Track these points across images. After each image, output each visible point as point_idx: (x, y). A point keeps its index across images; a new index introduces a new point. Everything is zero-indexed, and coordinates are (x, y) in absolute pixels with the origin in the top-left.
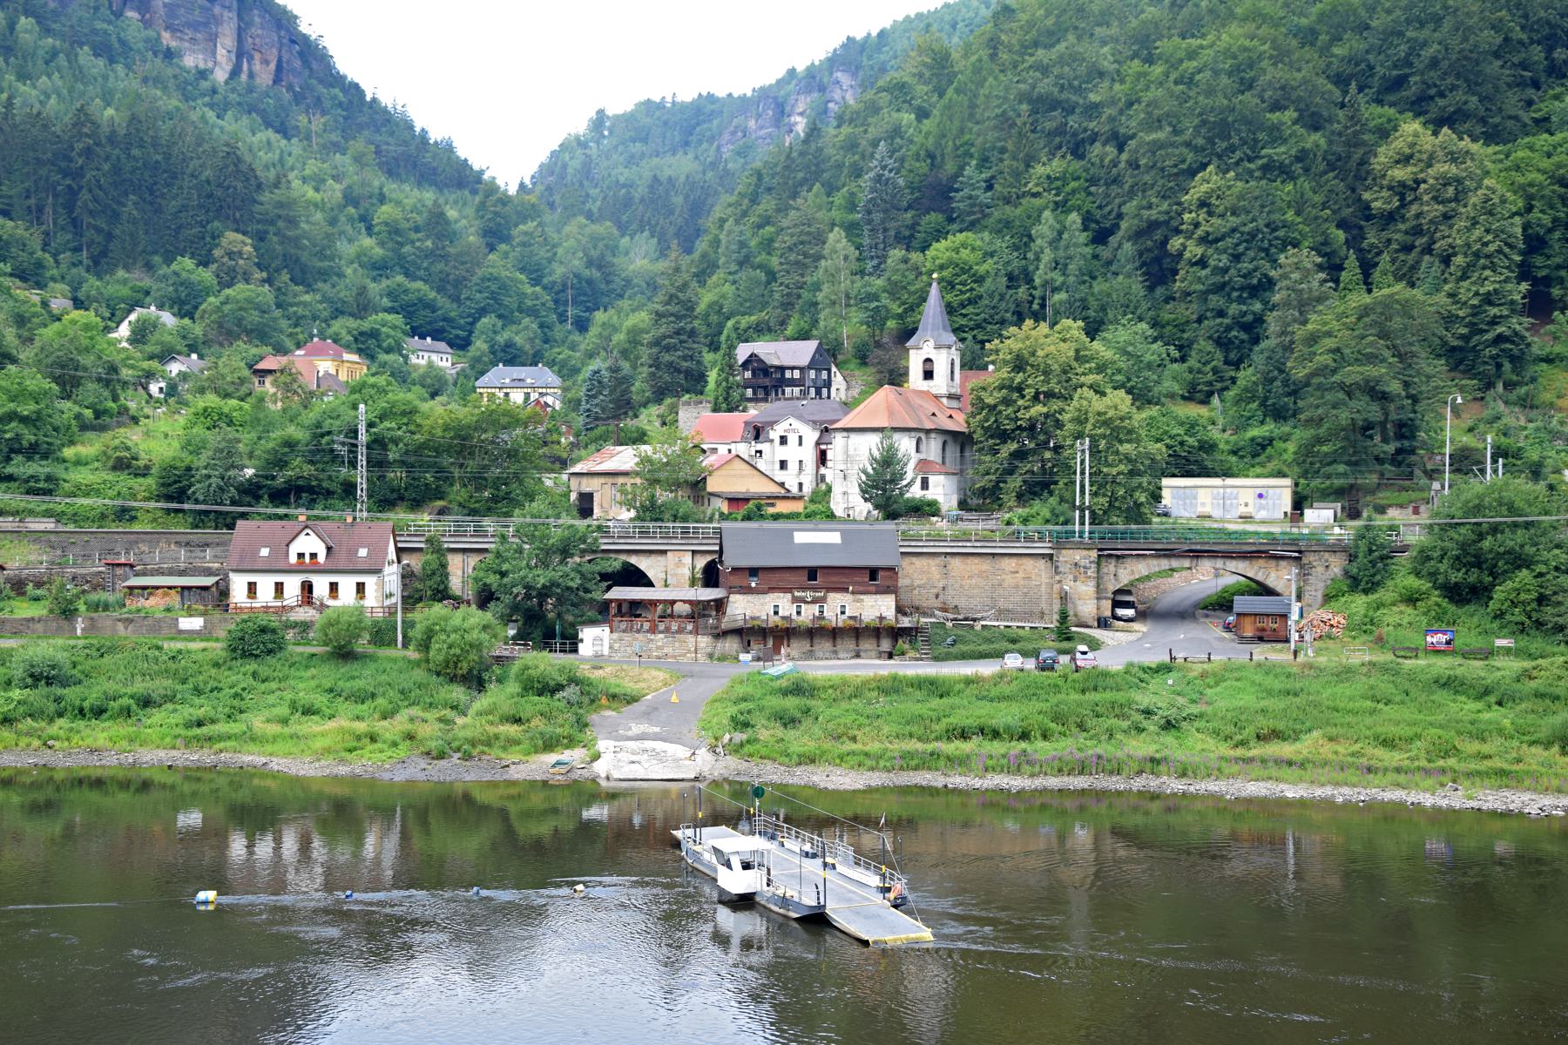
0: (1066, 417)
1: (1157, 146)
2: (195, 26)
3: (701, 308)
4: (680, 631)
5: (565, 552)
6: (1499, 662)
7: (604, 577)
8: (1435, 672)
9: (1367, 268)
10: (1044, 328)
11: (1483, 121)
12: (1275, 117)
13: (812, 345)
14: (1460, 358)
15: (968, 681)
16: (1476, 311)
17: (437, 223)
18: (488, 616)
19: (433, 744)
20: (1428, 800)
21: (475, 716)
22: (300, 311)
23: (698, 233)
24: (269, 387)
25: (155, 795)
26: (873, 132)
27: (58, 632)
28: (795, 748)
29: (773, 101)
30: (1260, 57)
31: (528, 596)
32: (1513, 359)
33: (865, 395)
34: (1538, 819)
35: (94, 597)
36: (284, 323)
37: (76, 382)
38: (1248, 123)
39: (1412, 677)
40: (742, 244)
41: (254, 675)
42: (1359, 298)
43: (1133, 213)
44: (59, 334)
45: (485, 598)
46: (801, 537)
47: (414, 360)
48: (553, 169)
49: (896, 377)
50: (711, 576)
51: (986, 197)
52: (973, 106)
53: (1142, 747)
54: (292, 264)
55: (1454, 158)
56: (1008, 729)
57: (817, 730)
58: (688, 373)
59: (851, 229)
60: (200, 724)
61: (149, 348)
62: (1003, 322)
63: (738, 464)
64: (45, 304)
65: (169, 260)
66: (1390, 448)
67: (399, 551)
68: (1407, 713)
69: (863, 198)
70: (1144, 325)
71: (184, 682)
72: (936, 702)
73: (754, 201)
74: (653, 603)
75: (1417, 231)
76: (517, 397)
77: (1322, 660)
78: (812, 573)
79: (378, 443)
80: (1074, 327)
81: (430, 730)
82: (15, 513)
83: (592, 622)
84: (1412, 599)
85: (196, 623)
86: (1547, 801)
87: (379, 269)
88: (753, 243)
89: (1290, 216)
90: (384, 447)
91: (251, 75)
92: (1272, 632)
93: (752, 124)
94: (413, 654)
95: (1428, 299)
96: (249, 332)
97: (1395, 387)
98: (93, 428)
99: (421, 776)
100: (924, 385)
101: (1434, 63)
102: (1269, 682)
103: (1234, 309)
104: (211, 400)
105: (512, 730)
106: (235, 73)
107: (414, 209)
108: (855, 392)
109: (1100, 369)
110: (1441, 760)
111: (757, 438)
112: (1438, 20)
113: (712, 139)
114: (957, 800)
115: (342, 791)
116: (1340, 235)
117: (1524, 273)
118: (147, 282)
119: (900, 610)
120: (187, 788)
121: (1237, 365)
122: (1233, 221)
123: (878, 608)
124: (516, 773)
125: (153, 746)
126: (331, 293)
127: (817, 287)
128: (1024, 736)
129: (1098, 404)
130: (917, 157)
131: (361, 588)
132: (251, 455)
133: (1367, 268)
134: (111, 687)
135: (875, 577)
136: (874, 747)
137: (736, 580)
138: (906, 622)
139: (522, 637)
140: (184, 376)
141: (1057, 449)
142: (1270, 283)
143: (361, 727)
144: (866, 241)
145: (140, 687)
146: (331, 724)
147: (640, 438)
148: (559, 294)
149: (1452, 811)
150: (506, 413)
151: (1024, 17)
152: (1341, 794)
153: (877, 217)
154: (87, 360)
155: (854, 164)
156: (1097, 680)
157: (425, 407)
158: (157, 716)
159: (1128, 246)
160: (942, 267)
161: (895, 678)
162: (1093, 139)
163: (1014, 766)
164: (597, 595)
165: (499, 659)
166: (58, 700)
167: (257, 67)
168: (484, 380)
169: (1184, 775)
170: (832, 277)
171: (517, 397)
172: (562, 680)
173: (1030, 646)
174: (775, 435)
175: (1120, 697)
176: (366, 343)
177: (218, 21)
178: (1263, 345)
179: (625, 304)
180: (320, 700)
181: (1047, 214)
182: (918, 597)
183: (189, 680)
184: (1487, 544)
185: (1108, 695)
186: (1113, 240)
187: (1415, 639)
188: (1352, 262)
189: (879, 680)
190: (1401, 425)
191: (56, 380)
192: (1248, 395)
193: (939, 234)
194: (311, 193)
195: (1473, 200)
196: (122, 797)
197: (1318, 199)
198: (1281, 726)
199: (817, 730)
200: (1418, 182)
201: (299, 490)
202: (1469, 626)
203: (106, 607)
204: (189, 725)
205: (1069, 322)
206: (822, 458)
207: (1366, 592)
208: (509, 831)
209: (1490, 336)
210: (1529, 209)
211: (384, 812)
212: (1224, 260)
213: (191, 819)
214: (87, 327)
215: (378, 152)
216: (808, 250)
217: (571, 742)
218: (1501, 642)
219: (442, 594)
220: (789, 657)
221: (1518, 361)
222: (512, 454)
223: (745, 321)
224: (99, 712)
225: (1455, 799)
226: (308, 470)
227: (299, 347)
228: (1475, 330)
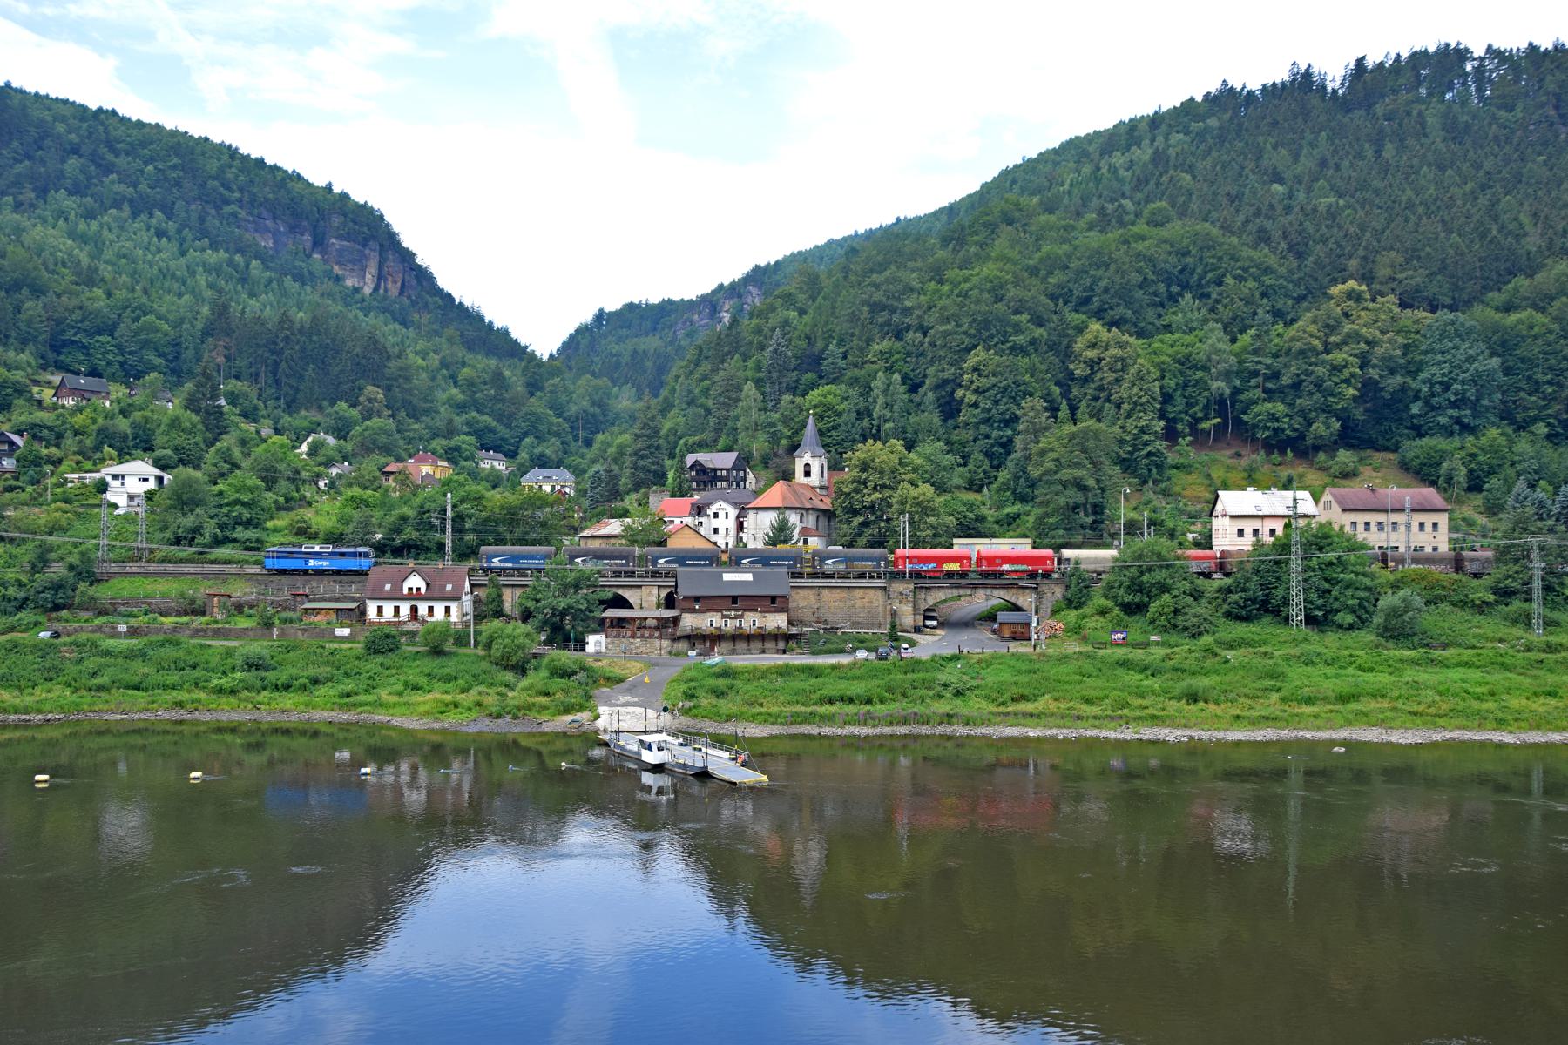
0: (894, 500)
1: (946, 334)
2: (353, 262)
3: (663, 432)
4: (651, 637)
5: (577, 587)
6: (1152, 650)
7: (602, 602)
8: (1116, 657)
9: (1073, 409)
10: (879, 444)
11: (1135, 325)
12: (1016, 318)
13: (734, 455)
14: (1127, 465)
15: (833, 667)
16: (1136, 437)
17: (498, 379)
18: (528, 628)
19: (494, 709)
20: (1112, 735)
21: (521, 691)
22: (412, 434)
23: (662, 384)
24: (391, 483)
25: (322, 739)
26: (771, 323)
27: (262, 637)
28: (724, 711)
29: (709, 303)
30: (1007, 282)
31: (553, 615)
32: (1157, 466)
33: (767, 486)
34: (1174, 744)
35: (284, 615)
36: (402, 442)
37: (275, 481)
38: (1001, 321)
39: (1103, 660)
40: (690, 392)
41: (382, 665)
42: (1069, 428)
43: (933, 374)
44: (266, 451)
45: (526, 616)
46: (727, 577)
47: (482, 465)
48: (572, 345)
49: (788, 476)
50: (670, 602)
51: (842, 364)
52: (834, 308)
53: (941, 707)
54: (407, 406)
55: (1120, 345)
56: (858, 696)
57: (738, 699)
58: (655, 472)
59: (758, 382)
60: (348, 695)
61: (319, 459)
62: (854, 441)
63: (687, 531)
64: (258, 432)
65: (333, 404)
66: (1089, 520)
67: (472, 586)
68: (1100, 683)
69: (766, 363)
70: (941, 444)
71: (338, 668)
72: (813, 681)
73: (697, 365)
74: (633, 619)
75: (1101, 388)
76: (547, 488)
77: (1051, 651)
78: (734, 599)
79: (459, 518)
80: (899, 445)
81: (491, 700)
82: (237, 562)
83: (595, 632)
84: (1103, 612)
85: (346, 632)
86: (1179, 733)
87: (461, 408)
88: (697, 391)
89: (1027, 377)
90: (463, 520)
91: (386, 290)
92: (1021, 635)
93: (696, 317)
94: (480, 652)
95: (1109, 430)
96: (380, 448)
97: (1091, 483)
98: (284, 509)
99: (486, 730)
100: (805, 480)
101: (1106, 290)
102: (1019, 665)
103: (995, 434)
104: (356, 491)
105: (543, 700)
106: (376, 289)
107: (484, 370)
108: (761, 484)
109: (915, 470)
110: (1119, 713)
111: (699, 514)
112: (1107, 266)
113: (671, 326)
114: (826, 742)
115: (437, 738)
116: (1057, 390)
117: (1162, 415)
118: (318, 418)
119: (790, 623)
120: (341, 735)
121: (997, 468)
122: (994, 380)
123: (777, 621)
124: (546, 728)
125: (320, 709)
126: (431, 423)
127: (737, 419)
128: (869, 701)
129: (913, 492)
130: (799, 338)
131: (448, 610)
132: (380, 526)
133: (1073, 409)
134: (294, 671)
135: (775, 602)
136: (774, 710)
137: (687, 605)
138: (794, 630)
139: (550, 640)
140: (339, 476)
141: (888, 520)
142: (1015, 419)
143: (448, 698)
144: (768, 390)
145: (312, 671)
146: (429, 696)
147: (624, 514)
148: (573, 423)
149: (1125, 741)
150: (540, 498)
151: (864, 255)
152: (1062, 733)
153: (775, 375)
154: (282, 467)
155: (760, 343)
156: (914, 665)
157: (489, 494)
158: (322, 690)
159: (930, 394)
160: (815, 407)
161: (787, 666)
162: (908, 329)
163: (862, 721)
164: (597, 614)
165: (535, 656)
166: (263, 679)
167: (390, 285)
168: (527, 477)
169: (967, 724)
170: (747, 412)
171: (547, 488)
172: (576, 668)
173: (872, 645)
174: (710, 512)
175: (928, 676)
176: (452, 455)
177: (367, 258)
178: (1013, 456)
179: (616, 429)
180: (422, 681)
181: (880, 374)
182: (801, 615)
183: (340, 667)
184: (1145, 578)
185: (921, 675)
186: (921, 391)
187: (1105, 637)
188: (1064, 406)
189: (778, 667)
190: (1095, 506)
191: (263, 479)
192: (1005, 487)
193: (814, 386)
194: (420, 361)
195: (1132, 371)
196: (303, 740)
197: (1043, 367)
198: (1026, 692)
199: (738, 699)
200: (1101, 359)
201: (409, 547)
202: (1137, 624)
203: (291, 622)
204: (341, 696)
205: (894, 441)
206: (740, 527)
207: (1076, 608)
208: (542, 763)
209: (1144, 452)
210: (1163, 377)
211: (462, 752)
212: (989, 404)
213: (345, 755)
214: (282, 446)
215: (462, 336)
216: (732, 393)
217: (581, 708)
218: (1153, 638)
219: (499, 613)
220: (720, 653)
221: (1160, 467)
222: (543, 524)
223: (691, 440)
224: (287, 687)
225: (1127, 734)
226: (415, 535)
227: (410, 457)
228: (1136, 449)
